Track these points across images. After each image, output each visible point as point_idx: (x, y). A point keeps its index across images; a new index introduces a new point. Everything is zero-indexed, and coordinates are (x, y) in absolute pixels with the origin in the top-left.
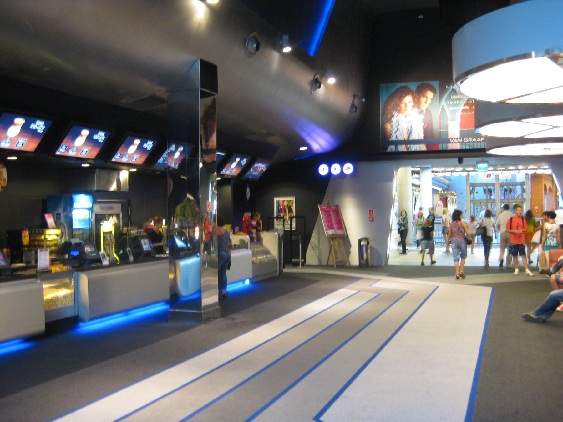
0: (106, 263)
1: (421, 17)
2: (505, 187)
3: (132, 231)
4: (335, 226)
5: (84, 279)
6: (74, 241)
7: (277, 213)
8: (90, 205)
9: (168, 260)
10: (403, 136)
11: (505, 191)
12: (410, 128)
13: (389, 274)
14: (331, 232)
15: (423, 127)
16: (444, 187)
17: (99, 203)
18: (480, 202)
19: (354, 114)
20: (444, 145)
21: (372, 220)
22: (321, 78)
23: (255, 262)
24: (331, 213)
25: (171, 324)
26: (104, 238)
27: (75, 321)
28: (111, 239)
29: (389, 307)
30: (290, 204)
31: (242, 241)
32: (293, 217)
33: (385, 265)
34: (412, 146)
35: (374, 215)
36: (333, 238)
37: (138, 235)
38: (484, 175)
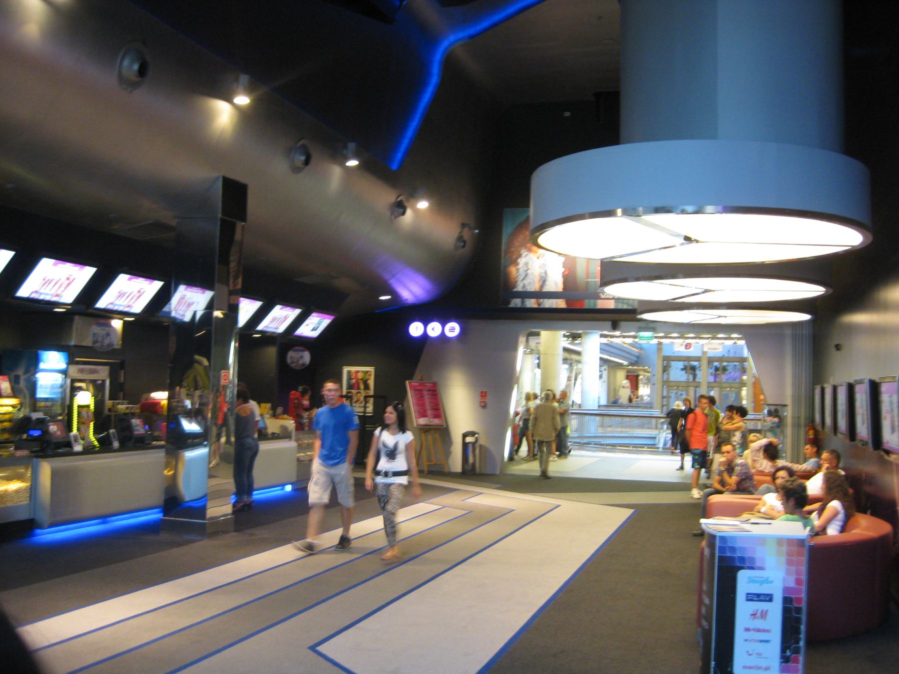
0: (78, 448)
1: (567, 114)
2: (716, 364)
3: (120, 406)
4: (429, 412)
5: (46, 469)
6: (35, 416)
7: (347, 389)
8: (63, 366)
9: (163, 450)
10: (532, 285)
11: (717, 369)
12: (544, 274)
13: (498, 486)
14: (422, 421)
15: (563, 273)
16: (631, 359)
17: (78, 363)
18: (678, 385)
19: (461, 251)
20: (592, 301)
21: (484, 406)
22: (408, 200)
23: (302, 459)
24: (425, 393)
25: (164, 536)
26: (79, 413)
27: (29, 526)
28: (88, 416)
29: (438, 525)
30: (367, 377)
31: (284, 428)
32: (370, 397)
33: (501, 472)
34: (546, 300)
35: (489, 399)
36: (425, 430)
37: (128, 411)
38: (682, 345)
